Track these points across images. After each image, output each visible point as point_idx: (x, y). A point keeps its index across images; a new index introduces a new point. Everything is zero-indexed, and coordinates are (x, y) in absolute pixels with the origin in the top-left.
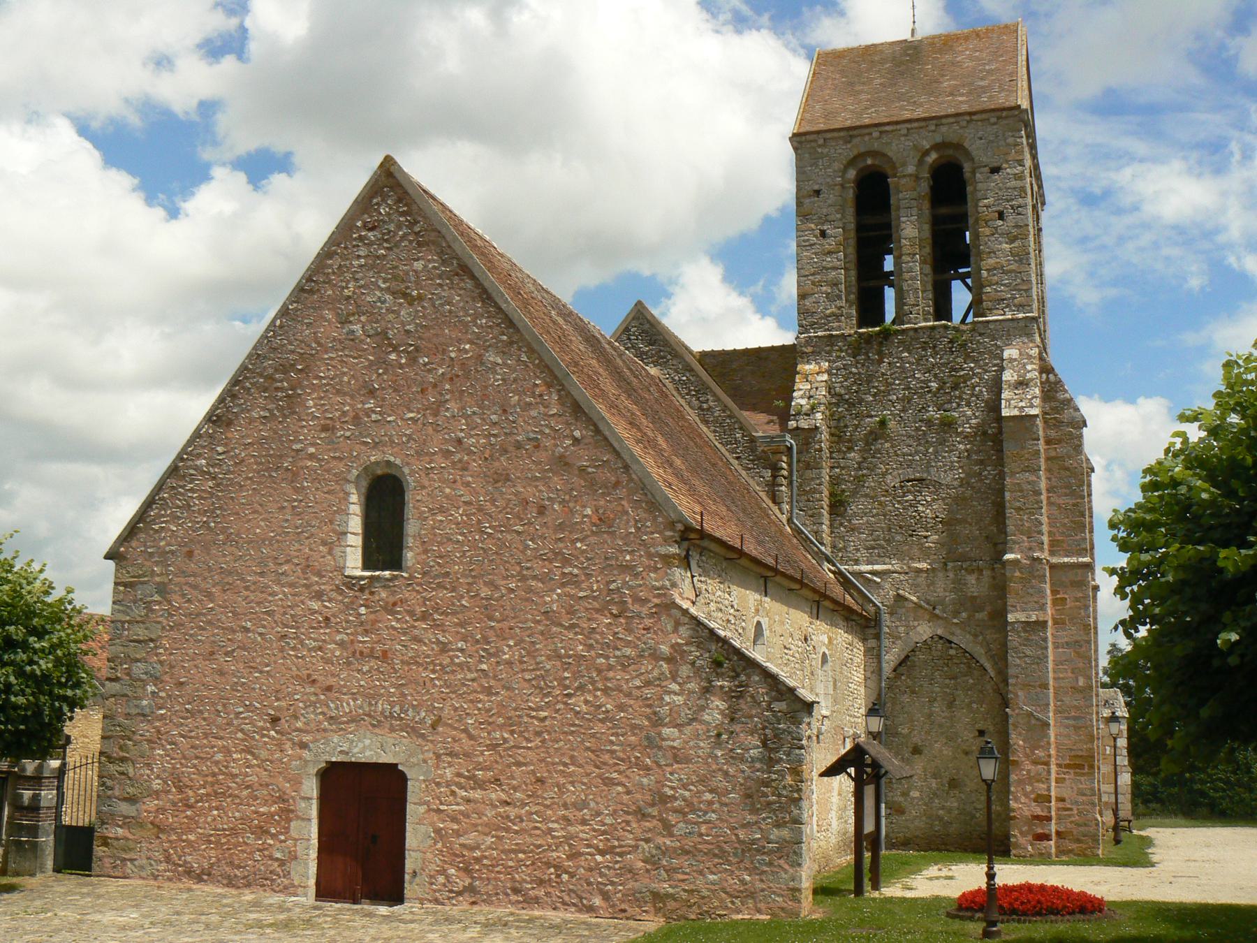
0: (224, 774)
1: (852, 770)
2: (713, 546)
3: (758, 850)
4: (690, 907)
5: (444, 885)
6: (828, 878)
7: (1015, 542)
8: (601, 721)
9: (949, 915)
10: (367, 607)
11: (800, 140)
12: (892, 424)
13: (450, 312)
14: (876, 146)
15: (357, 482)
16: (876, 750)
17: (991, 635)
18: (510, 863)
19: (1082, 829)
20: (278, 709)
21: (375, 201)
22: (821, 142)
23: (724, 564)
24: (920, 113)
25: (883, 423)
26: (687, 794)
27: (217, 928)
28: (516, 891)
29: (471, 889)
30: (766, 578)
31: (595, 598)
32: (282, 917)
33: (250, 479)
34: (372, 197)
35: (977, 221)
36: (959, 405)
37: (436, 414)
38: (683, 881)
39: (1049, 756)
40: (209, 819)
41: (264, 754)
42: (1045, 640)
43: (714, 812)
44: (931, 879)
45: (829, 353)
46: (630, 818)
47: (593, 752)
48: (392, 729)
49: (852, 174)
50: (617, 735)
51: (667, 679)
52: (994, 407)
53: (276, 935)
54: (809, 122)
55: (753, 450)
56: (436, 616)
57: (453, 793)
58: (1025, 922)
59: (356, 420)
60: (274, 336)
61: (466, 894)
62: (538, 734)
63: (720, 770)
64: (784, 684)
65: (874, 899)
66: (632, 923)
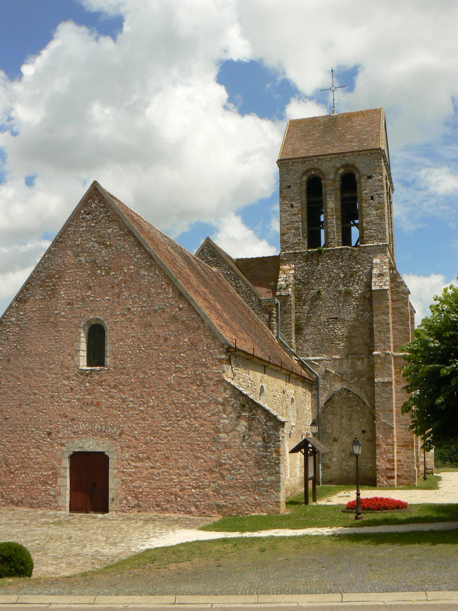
0: (27, 458)
1: (303, 450)
2: (241, 354)
3: (262, 486)
4: (233, 510)
5: (126, 504)
6: (295, 497)
7: (378, 347)
8: (193, 431)
9: (343, 511)
10: (89, 383)
11: (281, 163)
12: (323, 293)
13: (124, 251)
14: (316, 166)
15: (84, 327)
16: (314, 442)
17: (368, 388)
18: (155, 494)
19: (409, 474)
20: (51, 429)
21: (89, 201)
22: (291, 163)
23: (246, 361)
24: (336, 151)
25: (319, 292)
26: (231, 462)
27: (29, 525)
28: (158, 506)
29: (138, 506)
30: (265, 366)
31: (190, 378)
32: (56, 520)
33: (36, 326)
34: (88, 200)
35: (361, 201)
36: (353, 284)
37: (118, 297)
38: (230, 499)
39: (393, 442)
40: (21, 478)
41: (45, 449)
42: (391, 390)
43: (242, 469)
44: (340, 497)
45: (295, 260)
46: (206, 473)
47: (190, 444)
48: (102, 437)
49: (305, 178)
50: (200, 437)
51: (221, 412)
52: (369, 285)
53: (56, 527)
54: (286, 154)
55: (260, 305)
56: (120, 387)
57: (129, 464)
58: (373, 513)
59: (83, 300)
60: (45, 262)
61: (136, 508)
62: (166, 437)
63: (245, 451)
64: (272, 414)
65: (312, 506)
66: (208, 518)
